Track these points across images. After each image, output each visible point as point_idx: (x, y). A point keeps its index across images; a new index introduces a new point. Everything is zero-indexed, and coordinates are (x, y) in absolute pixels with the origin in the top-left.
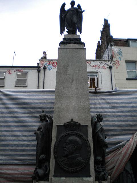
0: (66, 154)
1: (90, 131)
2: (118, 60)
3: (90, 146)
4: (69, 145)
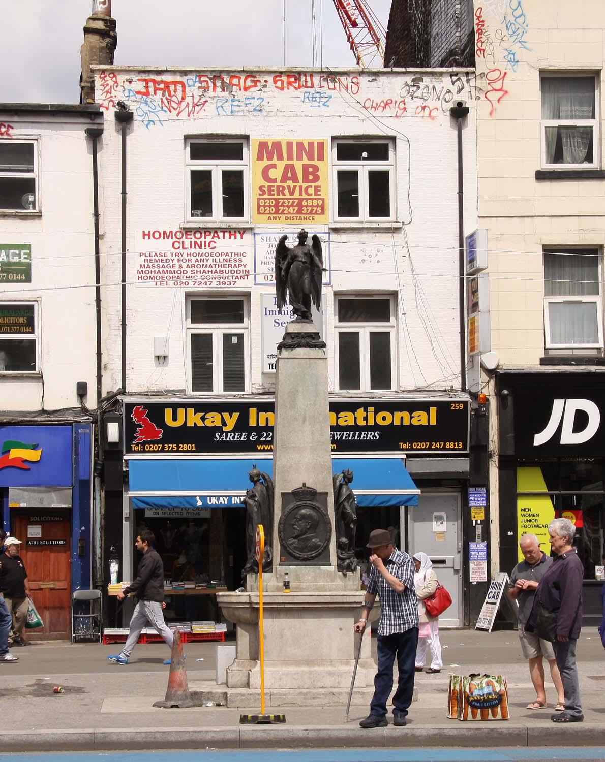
0: (296, 534)
1: (331, 500)
2: (503, 66)
3: (330, 523)
4: (300, 522)
